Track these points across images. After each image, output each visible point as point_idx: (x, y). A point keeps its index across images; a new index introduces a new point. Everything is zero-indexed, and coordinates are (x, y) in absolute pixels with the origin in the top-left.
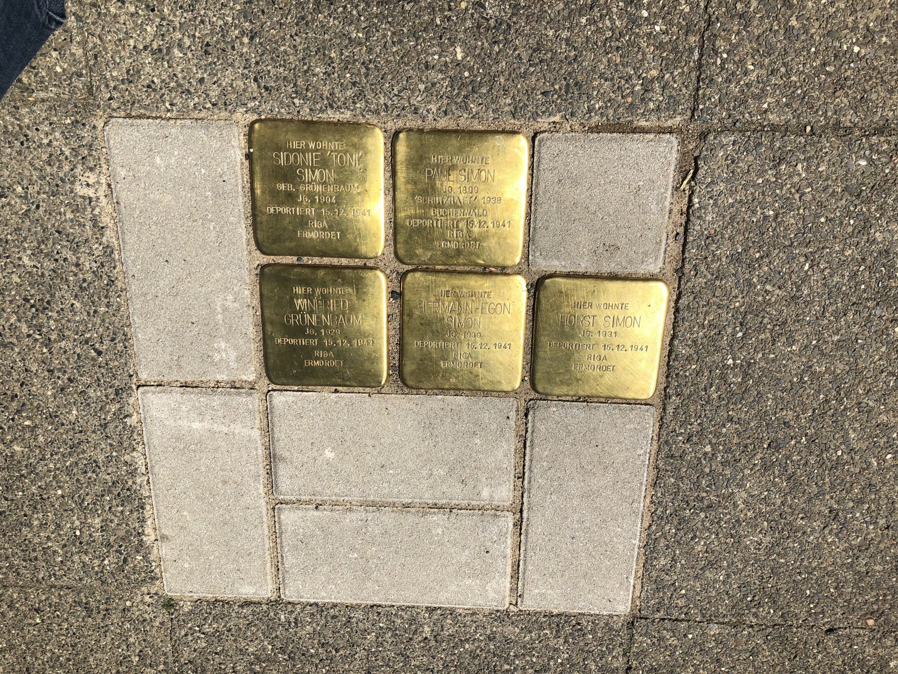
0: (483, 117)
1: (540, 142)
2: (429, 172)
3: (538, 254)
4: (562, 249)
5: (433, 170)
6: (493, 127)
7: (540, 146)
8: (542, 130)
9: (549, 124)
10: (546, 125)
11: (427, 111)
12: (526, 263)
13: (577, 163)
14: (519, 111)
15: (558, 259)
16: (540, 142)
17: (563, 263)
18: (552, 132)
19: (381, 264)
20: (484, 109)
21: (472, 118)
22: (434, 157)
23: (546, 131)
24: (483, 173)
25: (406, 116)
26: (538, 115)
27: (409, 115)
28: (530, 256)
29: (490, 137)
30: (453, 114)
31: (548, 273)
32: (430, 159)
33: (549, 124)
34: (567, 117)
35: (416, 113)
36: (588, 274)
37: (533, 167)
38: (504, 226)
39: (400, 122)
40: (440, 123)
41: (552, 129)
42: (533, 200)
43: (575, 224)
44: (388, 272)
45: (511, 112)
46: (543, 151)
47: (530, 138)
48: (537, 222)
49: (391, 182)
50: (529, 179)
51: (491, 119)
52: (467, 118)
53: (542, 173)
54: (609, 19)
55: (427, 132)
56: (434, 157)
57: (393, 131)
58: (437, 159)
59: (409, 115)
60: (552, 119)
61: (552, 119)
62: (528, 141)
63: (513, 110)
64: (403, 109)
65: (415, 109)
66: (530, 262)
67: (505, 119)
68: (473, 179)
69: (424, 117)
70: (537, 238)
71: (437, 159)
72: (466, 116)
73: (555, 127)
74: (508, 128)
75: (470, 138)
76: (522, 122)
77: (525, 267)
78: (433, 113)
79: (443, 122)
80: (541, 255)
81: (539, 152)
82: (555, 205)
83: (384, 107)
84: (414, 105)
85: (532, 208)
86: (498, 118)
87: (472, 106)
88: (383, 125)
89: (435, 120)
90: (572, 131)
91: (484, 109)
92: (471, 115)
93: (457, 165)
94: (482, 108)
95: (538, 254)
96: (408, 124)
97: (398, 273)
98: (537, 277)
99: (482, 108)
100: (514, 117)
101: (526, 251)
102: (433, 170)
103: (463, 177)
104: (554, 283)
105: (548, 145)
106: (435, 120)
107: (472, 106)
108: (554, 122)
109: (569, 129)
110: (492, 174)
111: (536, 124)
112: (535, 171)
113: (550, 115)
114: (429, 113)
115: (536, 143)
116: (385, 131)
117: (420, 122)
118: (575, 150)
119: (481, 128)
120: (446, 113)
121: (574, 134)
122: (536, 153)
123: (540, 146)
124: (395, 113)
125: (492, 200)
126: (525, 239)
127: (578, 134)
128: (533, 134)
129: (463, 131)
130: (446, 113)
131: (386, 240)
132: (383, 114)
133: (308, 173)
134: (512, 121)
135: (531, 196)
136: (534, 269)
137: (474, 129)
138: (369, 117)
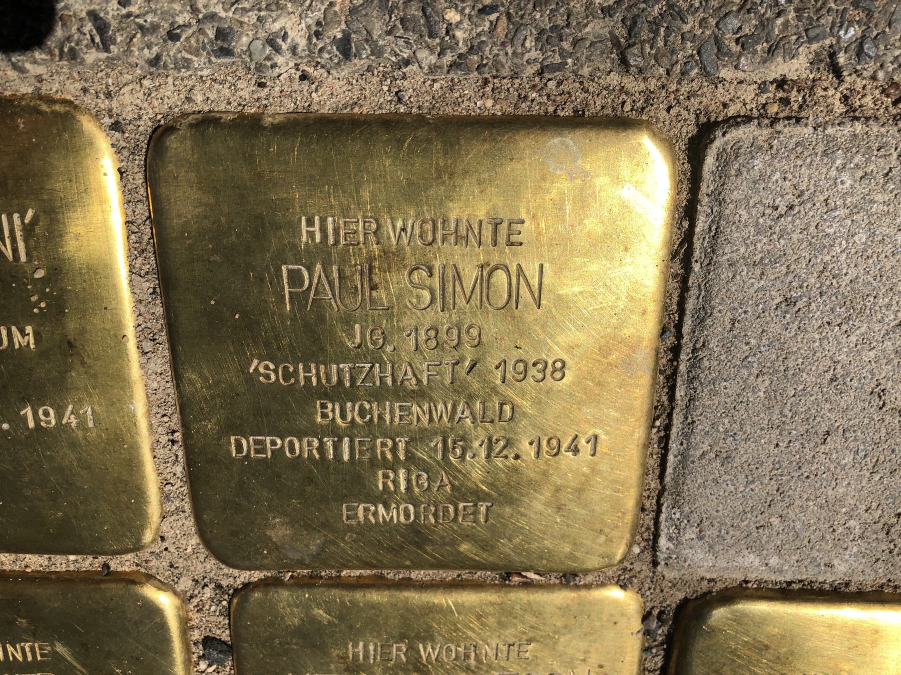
0: (497, 65)
1: (724, 161)
2: (296, 279)
3: (690, 533)
4: (775, 521)
5: (310, 270)
6: (537, 103)
7: (722, 172)
8: (732, 111)
9: (762, 88)
10: (748, 93)
11: (271, 42)
12: (648, 556)
13: (861, 237)
14: (645, 35)
15: (756, 547)
16: (724, 161)
17: (774, 561)
18: (775, 120)
19: (157, 566)
20: (501, 30)
21: (453, 66)
22: (310, 223)
23: (748, 119)
24: (500, 277)
25: (187, 64)
26: (720, 49)
27: (197, 61)
28: (663, 542)
29: (571, 140)
30: (377, 52)
31: (719, 586)
32: (297, 232)
33: (762, 88)
34: (842, 59)
35: (226, 52)
36: (853, 588)
37: (689, 253)
38: (576, 451)
39: (168, 90)
40: (325, 90)
41: (773, 109)
42: (682, 368)
43: (830, 445)
44: (185, 584)
45: (616, 43)
46: (735, 195)
47: (682, 145)
48: (696, 439)
49: (159, 310)
50: (667, 294)
51: (530, 70)
52: (433, 69)
53: (726, 274)
54: (551, 10)
55: (277, 128)
56: (310, 223)
57: (145, 125)
58: (323, 230)
59: (197, 61)
60: (780, 68)
61: (780, 68)
62: (674, 159)
63: (621, 32)
64: (173, 36)
65: (221, 34)
66: (661, 556)
67: (586, 71)
68: (461, 302)
69: (259, 68)
70: (691, 485)
71: (323, 230)
72: (427, 58)
73: (785, 102)
74: (596, 105)
75: (450, 147)
76: (653, 84)
77: (643, 568)
78: (294, 49)
79: (339, 86)
80: (701, 538)
81: (718, 198)
82: (764, 384)
83: (89, 27)
84: (212, 17)
85: (680, 393)
86: (561, 66)
87: (453, 16)
88: (104, 104)
89: (304, 77)
90: (852, 114)
91: (501, 30)
92: (448, 58)
93: (399, 252)
94: (494, 26)
95: (690, 533)
96: (199, 98)
97: (219, 586)
98: (680, 596)
99: (494, 26)
100: (624, 62)
101: (648, 520)
102: (310, 270)
103: (426, 295)
104: (739, 619)
105: (756, 173)
106: (304, 77)
107: (453, 16)
108: (781, 83)
109: (839, 108)
110: (535, 282)
111: (708, 89)
112: (696, 267)
113: (771, 51)
114: (277, 50)
115: (710, 162)
116: (116, 126)
117: (246, 89)
118: (861, 189)
119: (488, 105)
120: (345, 48)
121: (859, 127)
122: (705, 200)
123: (722, 172)
124: (141, 54)
125: (533, 371)
126: (643, 486)
127: (875, 128)
128: (692, 130)
129: (420, 120)
130: (345, 48)
131: (166, 498)
132: (92, 56)
133: (15, 250)
134: (614, 79)
135: (676, 350)
136: (671, 575)
137: (461, 111)
138: (41, 70)
